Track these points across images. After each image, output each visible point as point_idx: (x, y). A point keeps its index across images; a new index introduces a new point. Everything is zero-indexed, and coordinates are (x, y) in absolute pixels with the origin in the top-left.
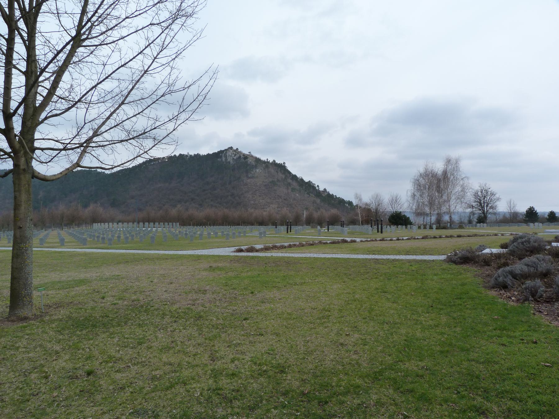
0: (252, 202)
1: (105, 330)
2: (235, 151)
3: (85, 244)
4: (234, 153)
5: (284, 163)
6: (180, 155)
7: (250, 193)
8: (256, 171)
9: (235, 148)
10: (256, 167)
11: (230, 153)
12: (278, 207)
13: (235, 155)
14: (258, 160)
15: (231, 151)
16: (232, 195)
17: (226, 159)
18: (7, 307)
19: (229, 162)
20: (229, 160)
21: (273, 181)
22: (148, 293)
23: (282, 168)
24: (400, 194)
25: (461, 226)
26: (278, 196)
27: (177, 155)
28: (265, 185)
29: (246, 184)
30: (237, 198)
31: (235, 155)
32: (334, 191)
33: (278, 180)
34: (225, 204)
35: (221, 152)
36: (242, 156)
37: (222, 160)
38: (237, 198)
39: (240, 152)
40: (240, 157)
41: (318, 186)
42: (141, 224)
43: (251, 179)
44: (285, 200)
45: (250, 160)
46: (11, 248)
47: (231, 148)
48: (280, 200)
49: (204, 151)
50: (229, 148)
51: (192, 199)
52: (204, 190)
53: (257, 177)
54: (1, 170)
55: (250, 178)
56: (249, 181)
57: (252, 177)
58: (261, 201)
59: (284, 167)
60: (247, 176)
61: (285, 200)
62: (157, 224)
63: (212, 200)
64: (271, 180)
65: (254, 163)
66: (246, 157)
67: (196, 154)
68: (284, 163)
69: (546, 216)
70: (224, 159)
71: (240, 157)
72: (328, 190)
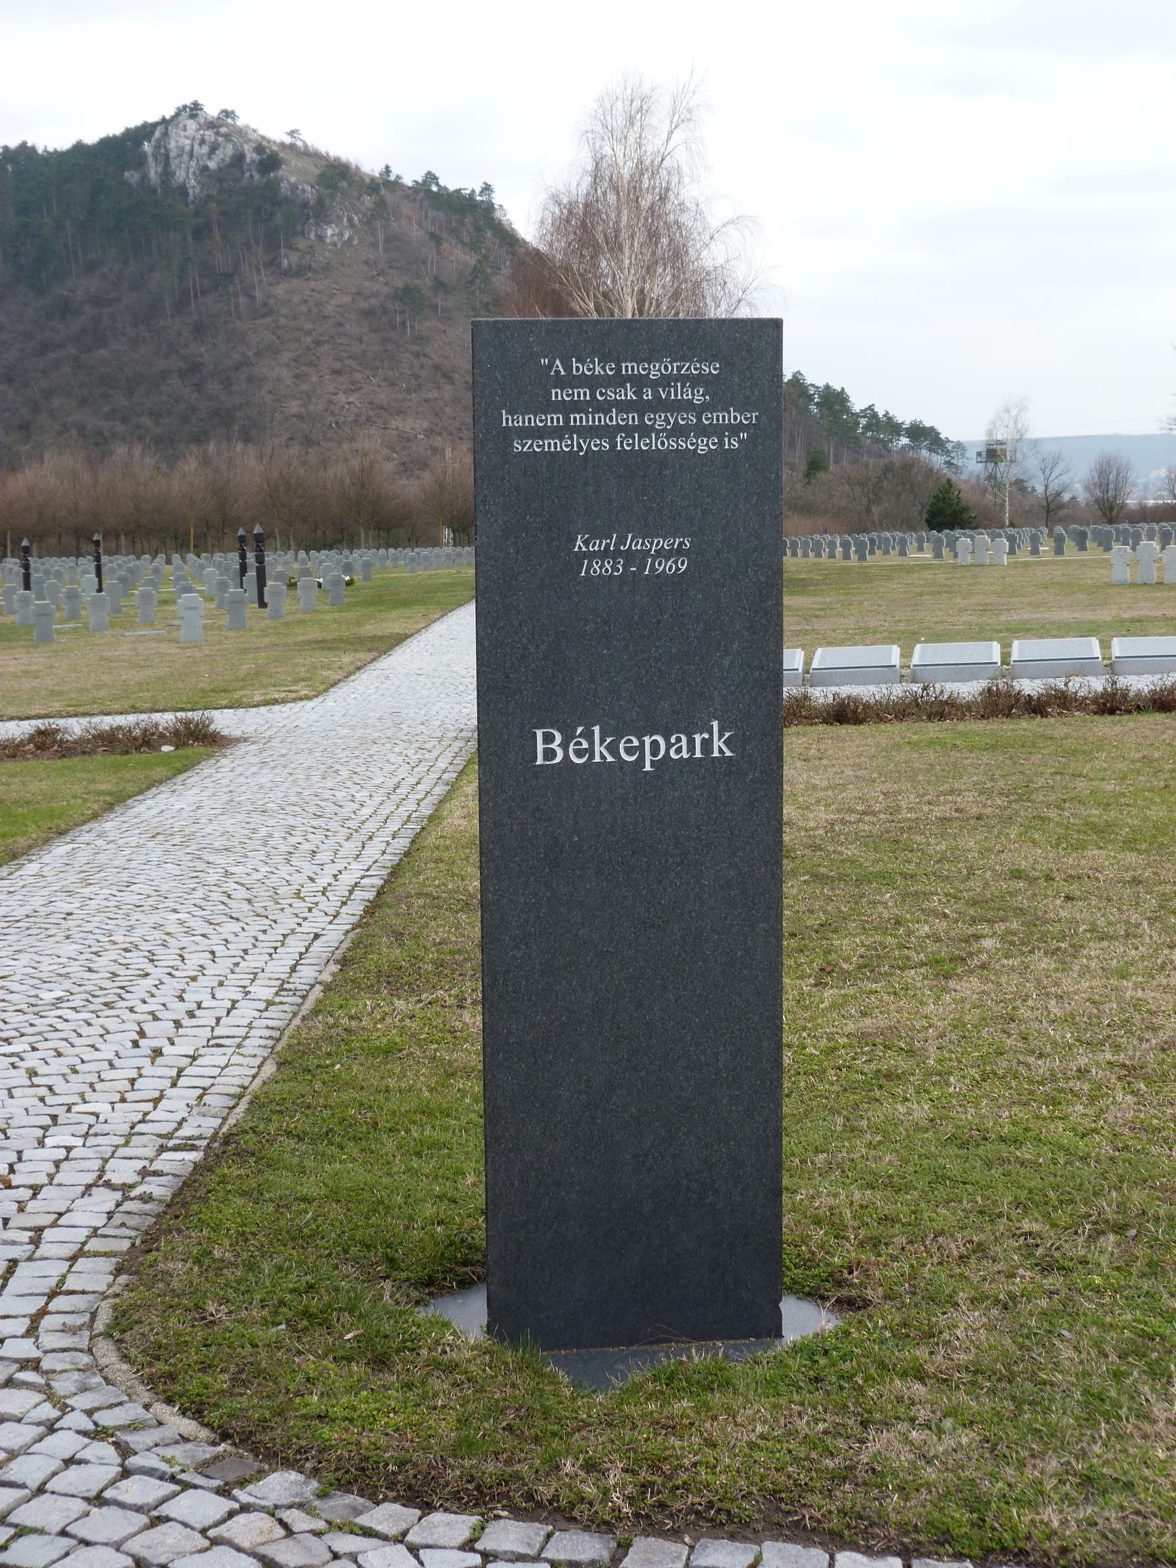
0: (294, 407)
2: (212, 125)
4: (209, 135)
7: (286, 357)
8: (321, 238)
9: (212, 110)
10: (320, 212)
12: (429, 432)
13: (214, 148)
14: (337, 174)
15: (192, 125)
16: (193, 368)
17: (167, 174)
19: (183, 190)
20: (180, 176)
21: (407, 290)
22: (1037, 805)
26: (437, 368)
28: (369, 313)
29: (268, 311)
30: (213, 386)
31: (214, 148)
33: (440, 286)
34: (147, 421)
35: (144, 132)
36: (250, 156)
37: (144, 178)
38: (213, 386)
39: (242, 133)
40: (239, 158)
43: (296, 283)
45: (289, 176)
47: (194, 110)
48: (447, 392)
52: (44, 348)
53: (327, 269)
54: (23, 157)
55: (288, 274)
56: (280, 290)
58: (342, 398)
59: (489, 208)
60: (273, 264)
63: (83, 402)
64: (399, 283)
65: (309, 193)
66: (270, 159)
68: (487, 188)
70: (154, 171)
71: (239, 158)
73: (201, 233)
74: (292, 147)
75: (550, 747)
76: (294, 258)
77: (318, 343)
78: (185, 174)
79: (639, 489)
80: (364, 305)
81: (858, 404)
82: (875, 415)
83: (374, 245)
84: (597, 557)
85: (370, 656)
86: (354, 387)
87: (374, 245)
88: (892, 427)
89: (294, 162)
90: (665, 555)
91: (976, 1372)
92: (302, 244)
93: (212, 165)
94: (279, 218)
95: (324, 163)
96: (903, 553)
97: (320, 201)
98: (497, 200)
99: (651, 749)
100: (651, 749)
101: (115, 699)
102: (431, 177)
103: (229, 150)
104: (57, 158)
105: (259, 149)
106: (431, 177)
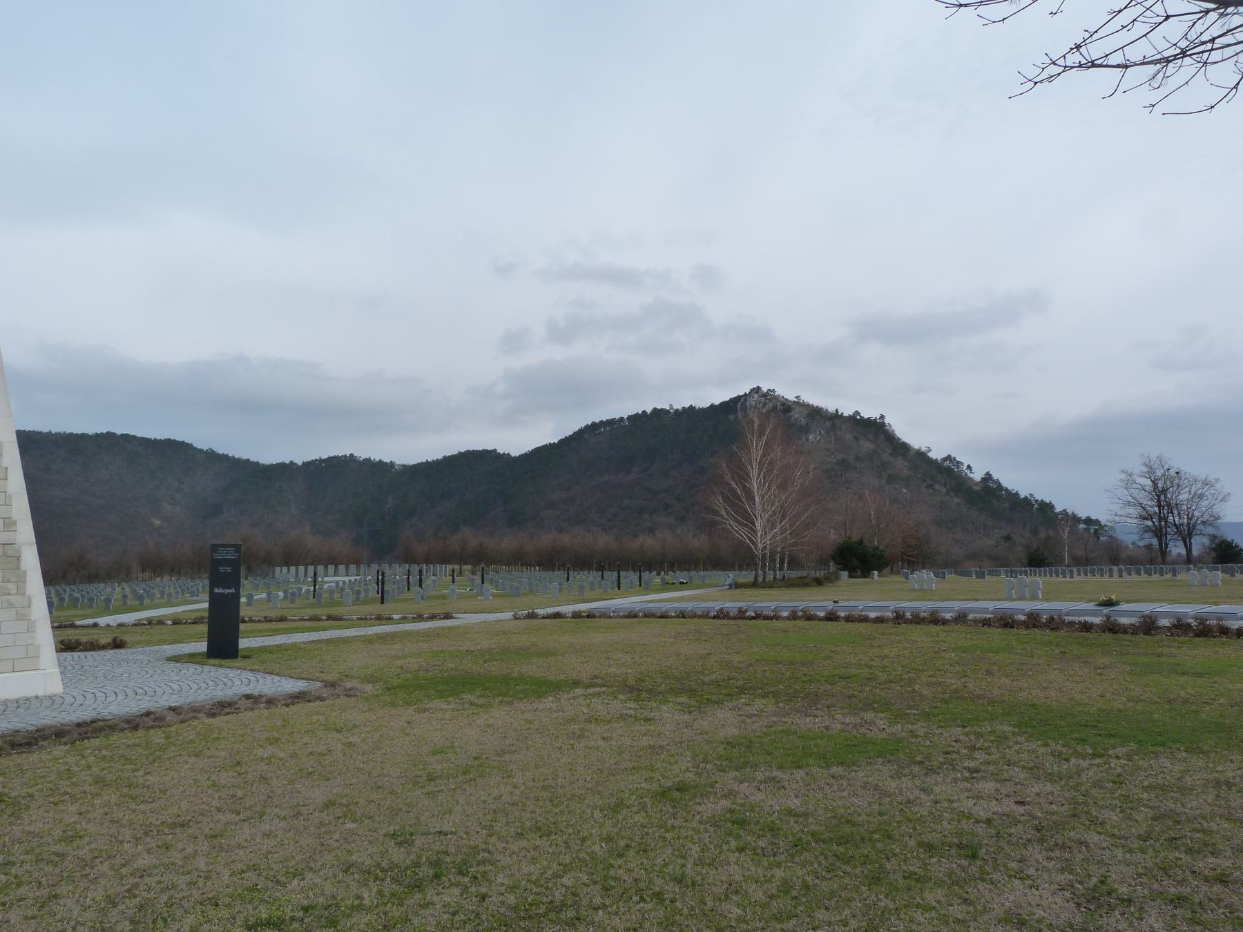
2: (765, 395)
5: (882, 417)
6: (655, 410)
9: (765, 390)
10: (805, 430)
11: (752, 402)
13: (765, 404)
14: (816, 413)
15: (756, 396)
21: (843, 460)
23: (876, 429)
24: (1094, 494)
25: (259, 621)
27: (649, 411)
31: (765, 404)
32: (1019, 480)
33: (858, 459)
35: (739, 398)
41: (969, 467)
42: (342, 568)
46: (206, 605)
50: (752, 391)
51: (667, 507)
59: (883, 424)
62: (342, 568)
64: (840, 457)
67: (687, 406)
68: (882, 417)
71: (775, 408)
72: (995, 477)
74: (798, 403)
75: (216, 590)
79: (226, 562)
81: (1058, 509)
82: (1067, 514)
84: (222, 569)
88: (1076, 519)
90: (229, 569)
96: (1072, 577)
98: (887, 421)
99: (227, 591)
100: (227, 591)
102: (857, 413)
104: (703, 410)
105: (783, 404)
106: (857, 413)
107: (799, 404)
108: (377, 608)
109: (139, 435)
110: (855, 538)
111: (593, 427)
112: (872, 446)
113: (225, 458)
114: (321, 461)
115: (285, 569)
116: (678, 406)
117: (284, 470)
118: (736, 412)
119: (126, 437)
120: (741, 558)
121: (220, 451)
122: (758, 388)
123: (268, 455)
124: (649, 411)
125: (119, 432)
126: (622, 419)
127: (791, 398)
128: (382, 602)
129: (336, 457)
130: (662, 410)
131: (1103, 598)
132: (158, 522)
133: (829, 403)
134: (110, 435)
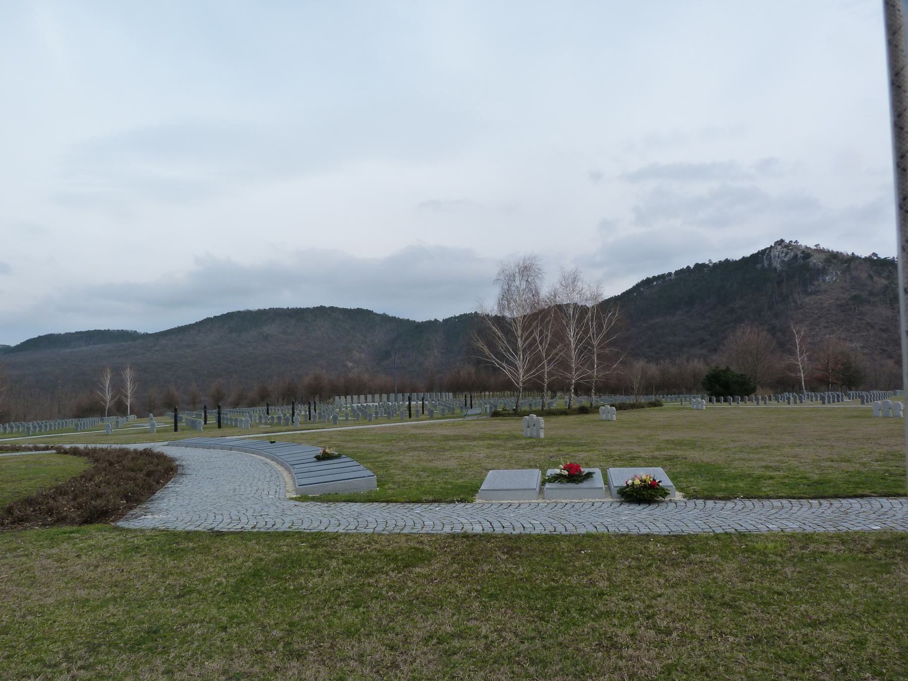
1: (51, 501)
2: (787, 246)
3: (370, 420)
6: (697, 265)
8: (824, 281)
9: (787, 241)
10: (823, 272)
12: (862, 348)
13: (787, 254)
15: (779, 247)
17: (770, 264)
18: (821, 504)
19: (775, 269)
26: (868, 324)
27: (692, 266)
28: (841, 306)
31: (787, 254)
33: (871, 294)
35: (762, 252)
36: (800, 255)
37: (763, 266)
40: (796, 256)
43: (813, 297)
44: (882, 330)
45: (814, 260)
48: (872, 333)
49: (737, 256)
50: (776, 243)
53: (825, 291)
56: (807, 299)
57: (815, 293)
61: (882, 330)
62: (377, 396)
66: (807, 254)
67: (723, 259)
69: (759, 390)
70: (766, 263)
71: (796, 256)
73: (779, 283)
76: (813, 287)
77: (819, 317)
78: (777, 264)
80: (839, 303)
83: (845, 281)
85: (644, 464)
86: (833, 332)
87: (845, 281)
89: (816, 255)
91: (110, 645)
92: (816, 283)
93: (786, 259)
94: (808, 275)
95: (823, 257)
97: (824, 268)
101: (425, 493)
103: (792, 254)
105: (803, 252)
107: (819, 251)
108: (291, 427)
109: (311, 306)
110: (723, 367)
111: (647, 282)
112: (886, 282)
113: (394, 319)
114: (455, 317)
115: (343, 397)
116: (715, 260)
117: (431, 325)
118: (762, 262)
119: (332, 308)
120: (508, 386)
121: (391, 314)
122: (782, 241)
123: (420, 317)
124: (692, 266)
125: (327, 306)
126: (670, 274)
127: (811, 244)
128: (219, 427)
129: (465, 315)
130: (703, 264)
131: (320, 452)
132: (350, 364)
133: (847, 248)
134: (322, 308)
